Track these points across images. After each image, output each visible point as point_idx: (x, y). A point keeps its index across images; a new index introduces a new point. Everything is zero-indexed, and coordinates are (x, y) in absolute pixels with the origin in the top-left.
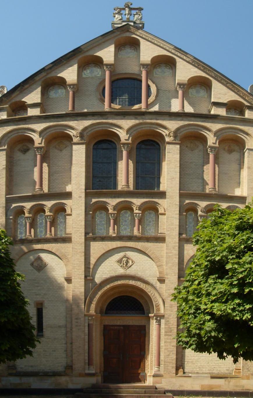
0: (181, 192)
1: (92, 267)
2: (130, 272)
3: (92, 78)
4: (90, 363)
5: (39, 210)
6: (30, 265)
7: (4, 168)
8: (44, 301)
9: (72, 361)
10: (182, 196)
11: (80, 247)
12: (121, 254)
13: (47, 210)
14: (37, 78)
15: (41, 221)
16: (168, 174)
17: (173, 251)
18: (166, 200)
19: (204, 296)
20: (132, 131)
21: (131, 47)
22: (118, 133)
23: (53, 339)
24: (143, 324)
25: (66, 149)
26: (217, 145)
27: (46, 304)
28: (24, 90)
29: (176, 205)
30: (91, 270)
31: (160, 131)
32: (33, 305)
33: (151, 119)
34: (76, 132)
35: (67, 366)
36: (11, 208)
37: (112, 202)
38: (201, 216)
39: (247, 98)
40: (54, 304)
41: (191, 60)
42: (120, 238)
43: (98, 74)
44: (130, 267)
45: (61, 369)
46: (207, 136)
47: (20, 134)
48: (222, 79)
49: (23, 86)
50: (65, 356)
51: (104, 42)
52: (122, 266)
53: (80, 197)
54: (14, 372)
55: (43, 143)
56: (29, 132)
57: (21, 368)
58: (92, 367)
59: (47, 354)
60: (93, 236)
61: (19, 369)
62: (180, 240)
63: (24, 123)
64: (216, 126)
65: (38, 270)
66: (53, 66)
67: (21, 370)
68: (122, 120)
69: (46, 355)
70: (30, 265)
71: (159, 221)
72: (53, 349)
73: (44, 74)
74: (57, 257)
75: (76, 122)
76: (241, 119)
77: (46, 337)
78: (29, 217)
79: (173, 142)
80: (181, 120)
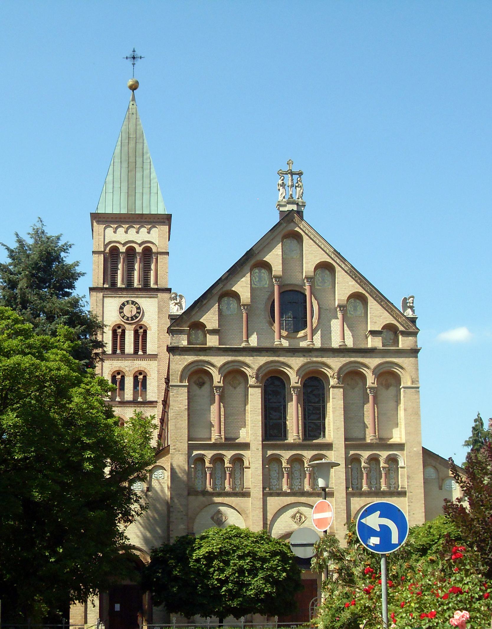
0: (346, 443)
1: (268, 523)
5: (218, 460)
7: (186, 409)
10: (347, 447)
11: (259, 503)
12: (295, 510)
13: (226, 461)
14: (215, 291)
16: (334, 423)
17: (341, 506)
18: (333, 452)
20: (301, 371)
22: (288, 373)
26: (375, 385)
28: (203, 306)
29: (342, 457)
30: (268, 526)
31: (325, 371)
33: (317, 357)
34: (252, 371)
36: (193, 455)
37: (286, 455)
38: (364, 468)
39: (400, 320)
41: (350, 269)
42: (293, 494)
44: (303, 522)
46: (366, 374)
48: (377, 295)
49: (202, 302)
51: (272, 239)
52: (296, 522)
53: (258, 449)
55: (222, 382)
56: (208, 366)
60: (269, 491)
62: (347, 494)
63: (204, 353)
64: (373, 362)
66: (229, 275)
68: (292, 358)
71: (336, 277)
73: (221, 285)
74: (236, 512)
75: (251, 358)
76: (395, 351)
78: (210, 468)
79: (337, 385)
80: (343, 357)
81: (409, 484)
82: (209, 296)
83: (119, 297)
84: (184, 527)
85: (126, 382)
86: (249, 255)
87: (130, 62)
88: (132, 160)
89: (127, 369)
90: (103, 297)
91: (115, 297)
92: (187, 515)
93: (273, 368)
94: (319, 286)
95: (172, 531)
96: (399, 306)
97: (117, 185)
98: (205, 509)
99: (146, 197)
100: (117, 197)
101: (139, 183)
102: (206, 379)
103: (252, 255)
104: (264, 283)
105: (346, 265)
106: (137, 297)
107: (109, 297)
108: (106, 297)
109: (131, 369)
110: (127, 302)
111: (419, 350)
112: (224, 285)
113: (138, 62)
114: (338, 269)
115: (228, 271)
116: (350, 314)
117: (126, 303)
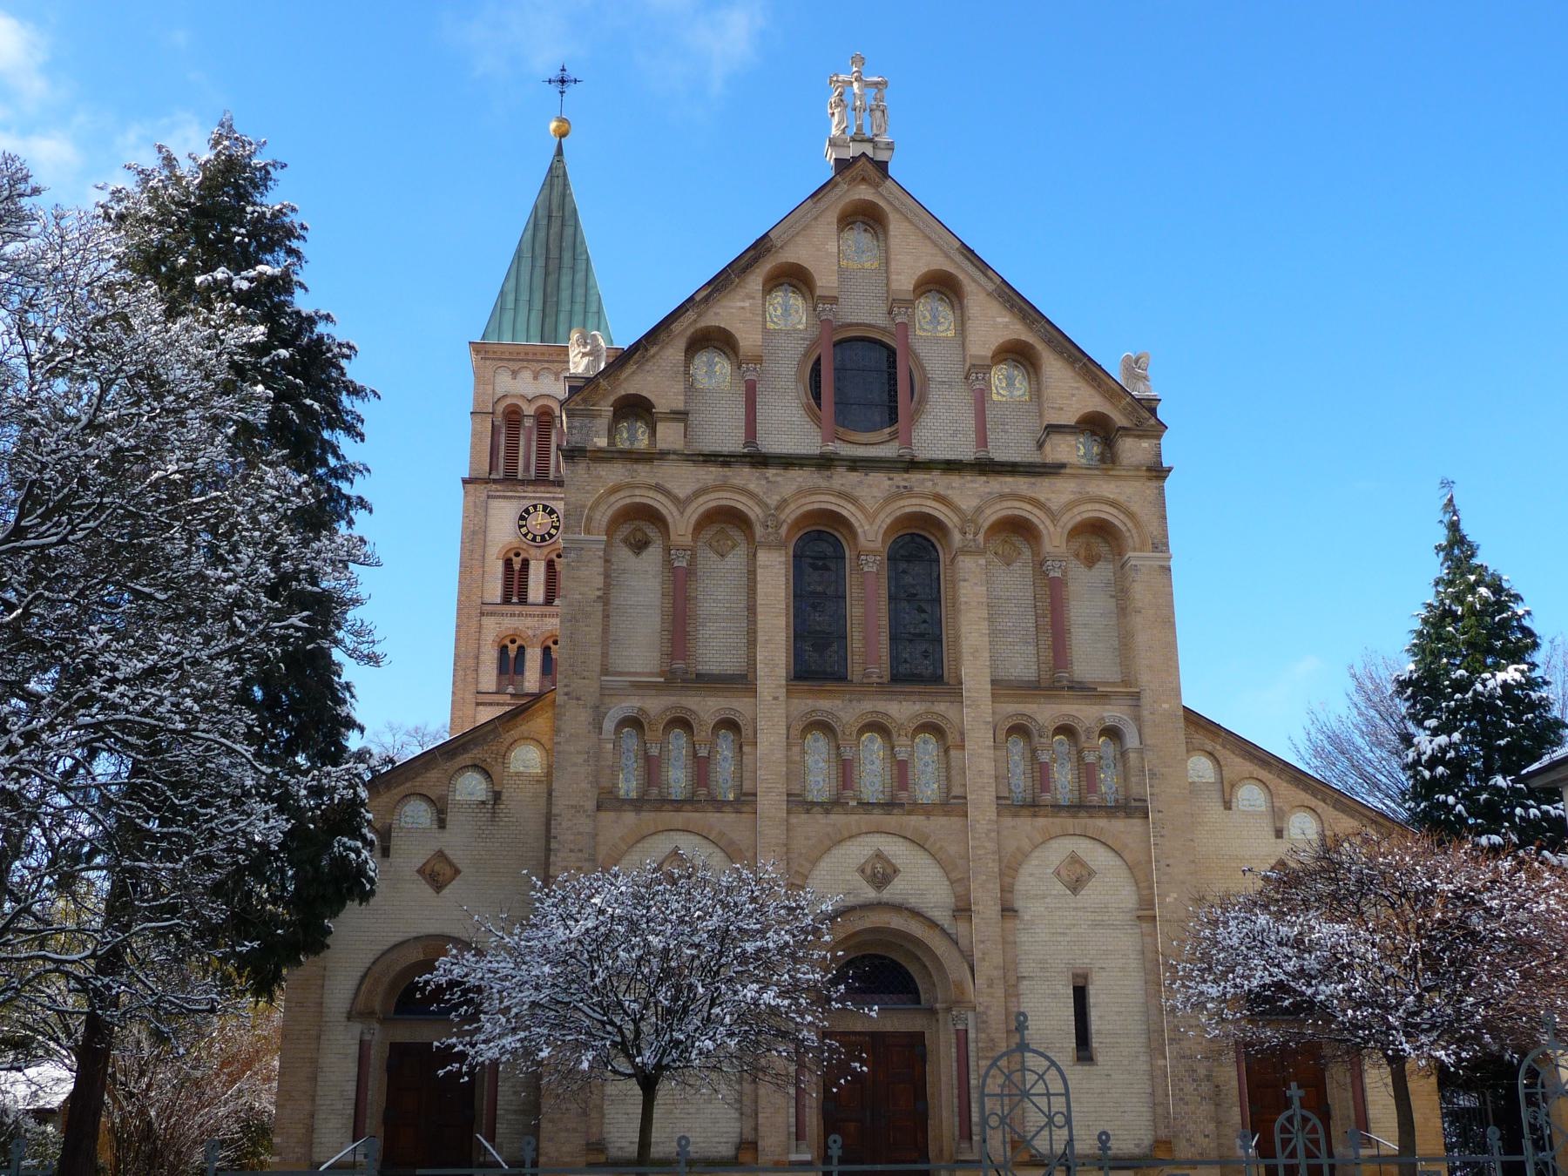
2: (893, 892)
3: (787, 333)
4: (799, 1135)
9: (756, 1129)
14: (677, 327)
24: (918, 1029)
35: (741, 1143)
43: (800, 322)
45: (726, 1150)
47: (637, 500)
50: (737, 1115)
51: (816, 219)
54: (602, 1158)
58: (803, 1147)
73: (691, 315)
81: (1156, 790)
82: (663, 336)
85: (528, 656)
86: (761, 248)
87: (554, 89)
88: (554, 253)
89: (530, 633)
90: (488, 497)
91: (511, 497)
93: (816, 506)
94: (925, 330)
96: (1116, 373)
97: (524, 297)
100: (522, 317)
101: (565, 294)
102: (652, 532)
103: (768, 250)
104: (794, 318)
105: (991, 279)
106: (554, 499)
107: (499, 497)
109: (538, 632)
111: (1170, 470)
112: (699, 315)
113: (571, 89)
114: (969, 287)
115: (709, 283)
116: (998, 393)
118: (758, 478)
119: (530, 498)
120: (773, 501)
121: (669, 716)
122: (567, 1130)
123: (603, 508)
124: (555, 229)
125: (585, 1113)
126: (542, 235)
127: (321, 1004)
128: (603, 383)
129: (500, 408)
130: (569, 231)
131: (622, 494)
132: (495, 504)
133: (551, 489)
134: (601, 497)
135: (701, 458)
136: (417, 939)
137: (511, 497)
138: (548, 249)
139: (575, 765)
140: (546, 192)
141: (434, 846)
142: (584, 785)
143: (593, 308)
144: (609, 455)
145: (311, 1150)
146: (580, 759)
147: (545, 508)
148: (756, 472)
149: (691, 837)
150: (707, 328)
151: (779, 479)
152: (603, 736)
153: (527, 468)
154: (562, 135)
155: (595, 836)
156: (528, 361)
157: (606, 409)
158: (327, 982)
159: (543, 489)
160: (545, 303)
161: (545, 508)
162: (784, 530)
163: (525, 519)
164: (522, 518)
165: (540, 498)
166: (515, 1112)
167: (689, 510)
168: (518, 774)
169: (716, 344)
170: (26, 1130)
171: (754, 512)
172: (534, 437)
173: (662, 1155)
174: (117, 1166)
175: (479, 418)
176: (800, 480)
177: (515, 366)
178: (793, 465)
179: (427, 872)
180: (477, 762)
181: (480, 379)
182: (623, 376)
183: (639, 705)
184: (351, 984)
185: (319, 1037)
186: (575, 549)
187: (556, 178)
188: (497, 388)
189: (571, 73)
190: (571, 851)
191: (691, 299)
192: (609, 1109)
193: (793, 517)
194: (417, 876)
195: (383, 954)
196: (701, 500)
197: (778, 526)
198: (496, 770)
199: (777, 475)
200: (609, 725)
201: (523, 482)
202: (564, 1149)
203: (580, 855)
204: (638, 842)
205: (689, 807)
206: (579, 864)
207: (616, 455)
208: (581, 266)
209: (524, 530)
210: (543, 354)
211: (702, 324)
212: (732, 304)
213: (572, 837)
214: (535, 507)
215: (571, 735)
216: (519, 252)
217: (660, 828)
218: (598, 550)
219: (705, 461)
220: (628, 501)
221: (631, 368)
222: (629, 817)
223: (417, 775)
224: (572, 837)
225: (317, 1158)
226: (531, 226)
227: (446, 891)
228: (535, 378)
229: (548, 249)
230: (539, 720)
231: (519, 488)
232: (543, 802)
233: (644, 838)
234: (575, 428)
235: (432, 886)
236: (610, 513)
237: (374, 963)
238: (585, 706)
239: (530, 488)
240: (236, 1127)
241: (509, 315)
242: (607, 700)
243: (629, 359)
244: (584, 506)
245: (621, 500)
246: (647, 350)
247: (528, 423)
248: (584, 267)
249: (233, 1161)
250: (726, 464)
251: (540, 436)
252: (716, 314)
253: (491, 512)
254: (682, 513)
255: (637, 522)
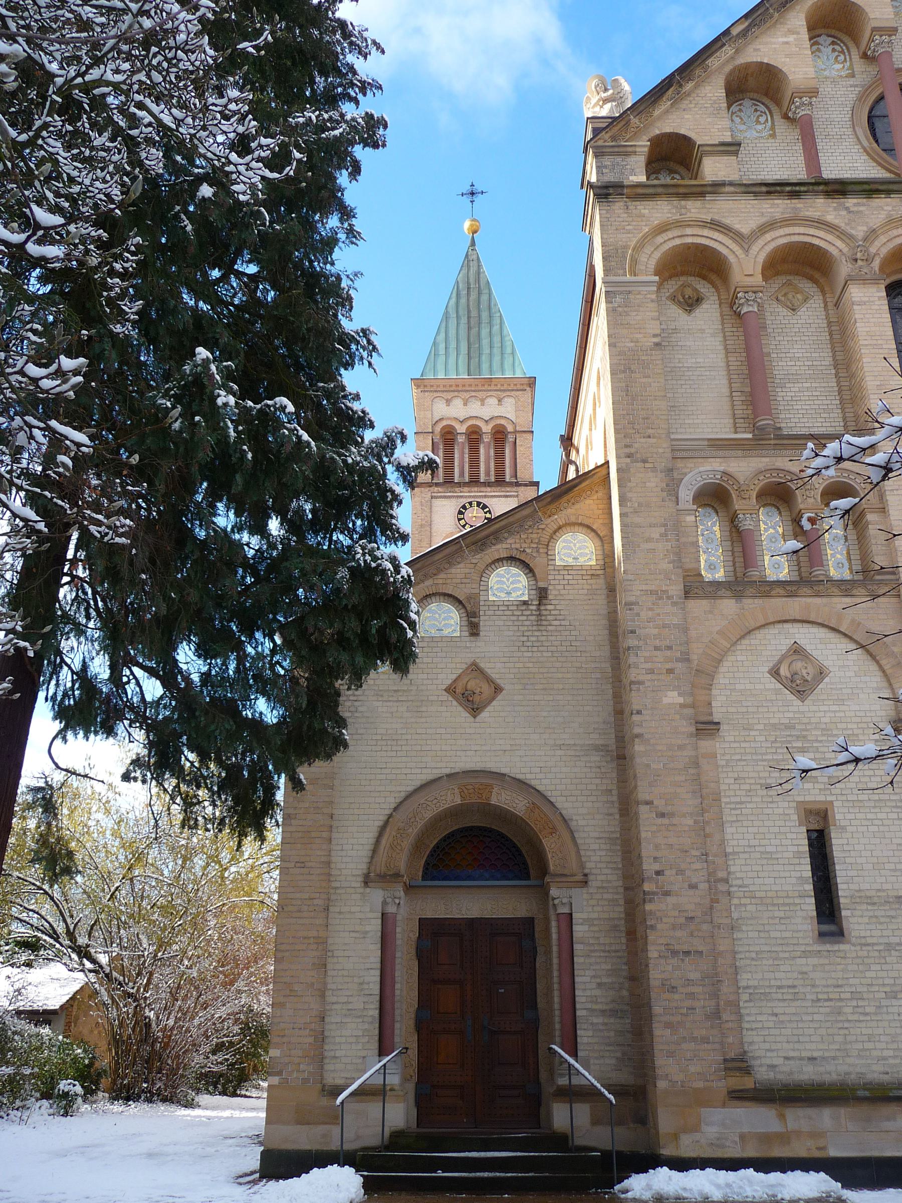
6: (770, 672)
8: (832, 802)
14: (714, 62)
15: (771, 531)
19: (80, 1100)
21: (833, 43)
23: (881, 948)
25: (807, 305)
27: (840, 815)
32: (795, 817)
40: (869, 816)
47: (690, 240)
54: (748, 1083)
57: (772, 1067)
59: (868, 1010)
61: (762, 1074)
65: (799, 692)
67: (771, 1075)
69: (867, 1014)
70: (770, 672)
72: (887, 989)
73: (728, 51)
77: (853, 940)
83: (457, 497)
84: (681, 700)
87: (466, 200)
88: (474, 313)
92: (685, 659)
95: (639, 712)
97: (453, 345)
98: (745, 642)
99: (497, 359)
101: (485, 342)
106: (485, 496)
108: (436, 497)
110: (470, 503)
112: (737, 51)
113: (478, 199)
115: (746, 16)
117: (467, 506)
118: (835, 209)
119: (466, 497)
120: (859, 231)
121: (763, 481)
122: (694, 1039)
123: (648, 249)
124: (474, 295)
125: (716, 1014)
126: (463, 301)
127: (329, 863)
128: (634, 121)
129: (438, 429)
130: (484, 298)
131: (670, 234)
132: (437, 503)
133: (483, 489)
134: (645, 237)
135: (764, 189)
136: (449, 776)
137: (453, 497)
138: (469, 312)
139: (649, 540)
140: (464, 271)
141: (468, 658)
142: (666, 566)
143: (508, 350)
144: (651, 191)
145: (322, 1068)
146: (655, 533)
147: (479, 504)
148: (833, 203)
149: (815, 630)
150: (748, 65)
151: (861, 208)
152: (681, 507)
153: (462, 474)
154: (475, 232)
155: (686, 630)
156: (458, 391)
157: (643, 144)
158: (334, 835)
159: (476, 489)
160: (469, 348)
161: (479, 504)
162: (876, 264)
163: (463, 514)
164: (460, 513)
165: (473, 497)
166: (603, 1012)
167: (755, 248)
168: (566, 568)
169: (752, 95)
170: (15, 1033)
171: (833, 245)
172: (467, 451)
173: (834, 1077)
174: (117, 1070)
175: (421, 437)
176: (890, 208)
177: (449, 396)
178: (878, 191)
179: (459, 690)
180: (514, 554)
181: (420, 406)
182: (657, 113)
183: (722, 468)
184: (367, 837)
185: (327, 909)
186: (621, 293)
187: (471, 261)
188: (435, 414)
189: (478, 187)
190: (657, 648)
191: (727, 32)
192: (749, 1010)
193: (884, 251)
194: (446, 697)
195: (407, 797)
196: (768, 236)
197: (869, 260)
198: (537, 563)
199: (858, 204)
200: (686, 494)
201: (459, 484)
202: (692, 1069)
203: (668, 653)
204: (743, 637)
205: (806, 590)
206: (669, 666)
207: (660, 190)
208: (496, 321)
209: (462, 522)
210: (470, 385)
211: (741, 60)
212: (773, 40)
213: (656, 631)
214: (470, 503)
215: (640, 505)
216: (446, 315)
217: (772, 620)
218: (649, 292)
219: (769, 193)
220: (678, 242)
221: (664, 105)
222: (728, 606)
223: (439, 571)
224: (656, 631)
225: (333, 1078)
226: (454, 295)
227: (484, 715)
228: (465, 404)
229: (469, 312)
230: (588, 502)
231: (457, 489)
232: (601, 600)
233: (749, 632)
234: (606, 167)
235: (465, 708)
236: (657, 255)
237: (395, 809)
238: (654, 469)
239: (466, 489)
240: (236, 1029)
241: (442, 359)
242: (680, 464)
243: (662, 95)
244: (626, 247)
245: (670, 241)
246: (681, 86)
247: (461, 439)
248: (498, 321)
249: (233, 1064)
250: (795, 195)
251: (470, 449)
252: (756, 50)
253: (434, 509)
254: (747, 251)
255: (683, 278)
